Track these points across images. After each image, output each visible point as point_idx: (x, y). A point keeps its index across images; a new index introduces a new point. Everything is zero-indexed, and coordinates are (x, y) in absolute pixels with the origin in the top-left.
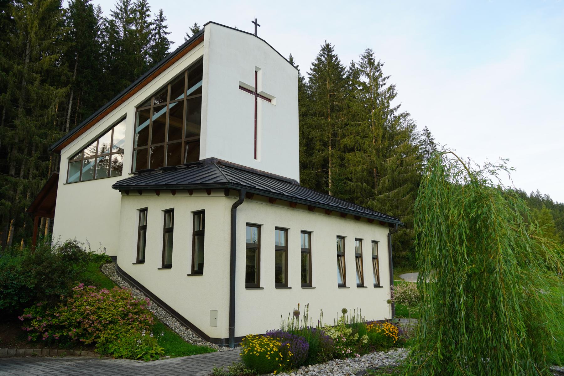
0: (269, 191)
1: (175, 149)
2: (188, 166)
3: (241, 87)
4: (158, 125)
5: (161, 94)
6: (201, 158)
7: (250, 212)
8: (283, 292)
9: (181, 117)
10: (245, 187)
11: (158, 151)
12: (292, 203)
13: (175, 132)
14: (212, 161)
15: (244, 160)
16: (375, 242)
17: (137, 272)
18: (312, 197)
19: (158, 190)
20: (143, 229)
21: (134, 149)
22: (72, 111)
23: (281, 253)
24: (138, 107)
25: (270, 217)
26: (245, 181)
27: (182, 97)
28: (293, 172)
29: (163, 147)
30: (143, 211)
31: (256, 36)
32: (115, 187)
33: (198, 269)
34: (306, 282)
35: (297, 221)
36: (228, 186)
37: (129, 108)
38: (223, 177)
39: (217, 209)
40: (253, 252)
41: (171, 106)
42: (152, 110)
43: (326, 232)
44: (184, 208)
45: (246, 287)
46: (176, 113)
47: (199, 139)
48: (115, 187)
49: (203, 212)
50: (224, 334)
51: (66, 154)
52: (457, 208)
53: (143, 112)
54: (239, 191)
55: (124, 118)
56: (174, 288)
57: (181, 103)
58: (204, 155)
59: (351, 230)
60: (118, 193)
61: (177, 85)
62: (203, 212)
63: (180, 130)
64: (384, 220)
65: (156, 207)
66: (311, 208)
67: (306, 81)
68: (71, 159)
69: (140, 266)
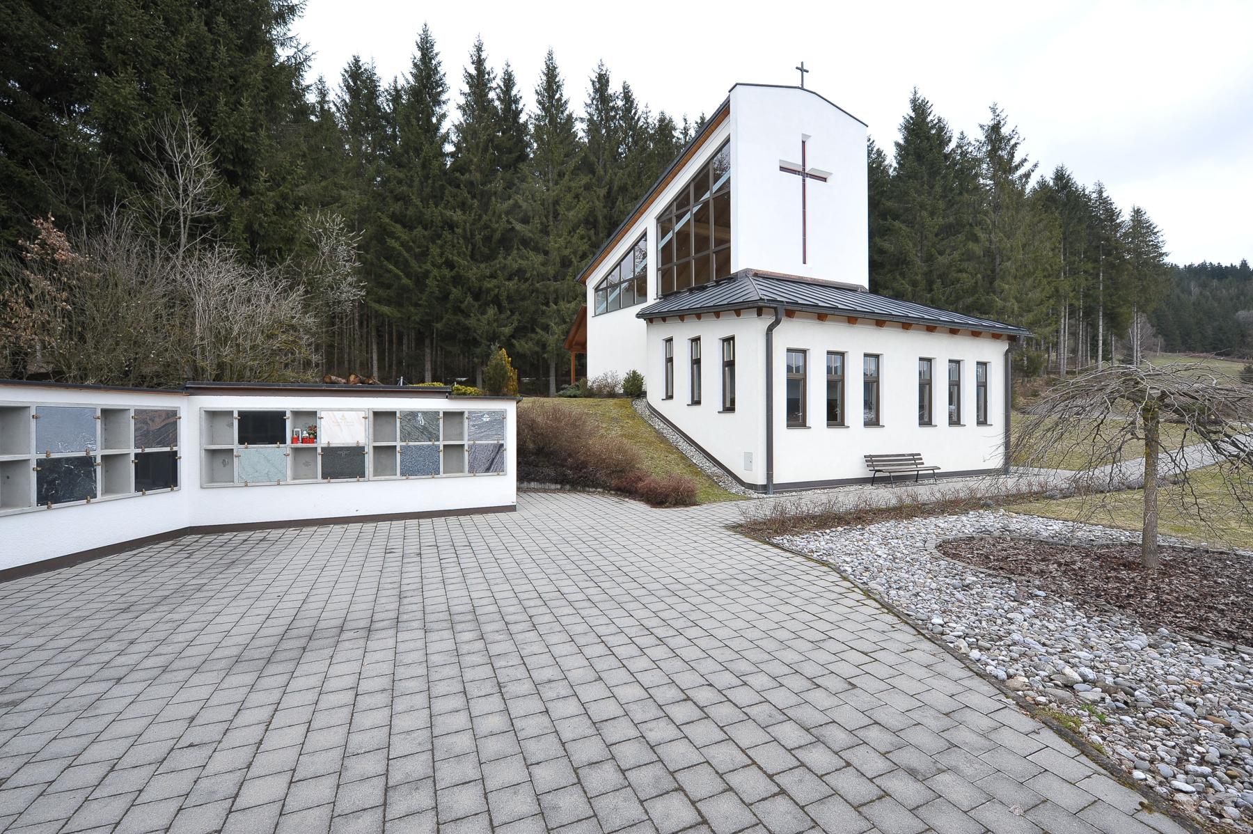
0: (817, 306)
1: (703, 264)
2: (718, 283)
3: (782, 169)
4: (683, 236)
5: (682, 201)
6: (733, 271)
7: (791, 334)
8: (837, 432)
9: (708, 222)
10: (785, 302)
11: (684, 269)
12: (852, 318)
13: (702, 242)
14: (746, 272)
15: (791, 267)
16: (982, 365)
17: (665, 408)
18: (881, 305)
19: (681, 316)
20: (670, 360)
21: (658, 270)
22: (1098, 329)
23: (835, 386)
24: (659, 219)
25: (817, 341)
26: (784, 294)
27: (707, 195)
28: (860, 276)
29: (689, 263)
30: (696, 340)
31: (802, 88)
32: (639, 316)
33: (729, 407)
34: (873, 421)
35: (856, 343)
36: (761, 304)
37: (648, 222)
38: (755, 291)
39: (750, 335)
40: (797, 385)
41: (695, 210)
42: (674, 219)
43: (901, 355)
44: (712, 334)
45: (789, 426)
46: (701, 218)
47: (729, 248)
48: (639, 316)
49: (733, 338)
50: (761, 480)
51: (592, 282)
52: (427, 342)
53: (664, 223)
54: (775, 309)
55: (644, 235)
56: (703, 425)
57: (706, 204)
58: (734, 269)
59: (942, 349)
60: (642, 322)
61: (701, 181)
62: (733, 338)
63: (707, 239)
64: (998, 331)
65: (682, 334)
66: (880, 321)
67: (891, 159)
68: (597, 289)
69: (669, 402)
